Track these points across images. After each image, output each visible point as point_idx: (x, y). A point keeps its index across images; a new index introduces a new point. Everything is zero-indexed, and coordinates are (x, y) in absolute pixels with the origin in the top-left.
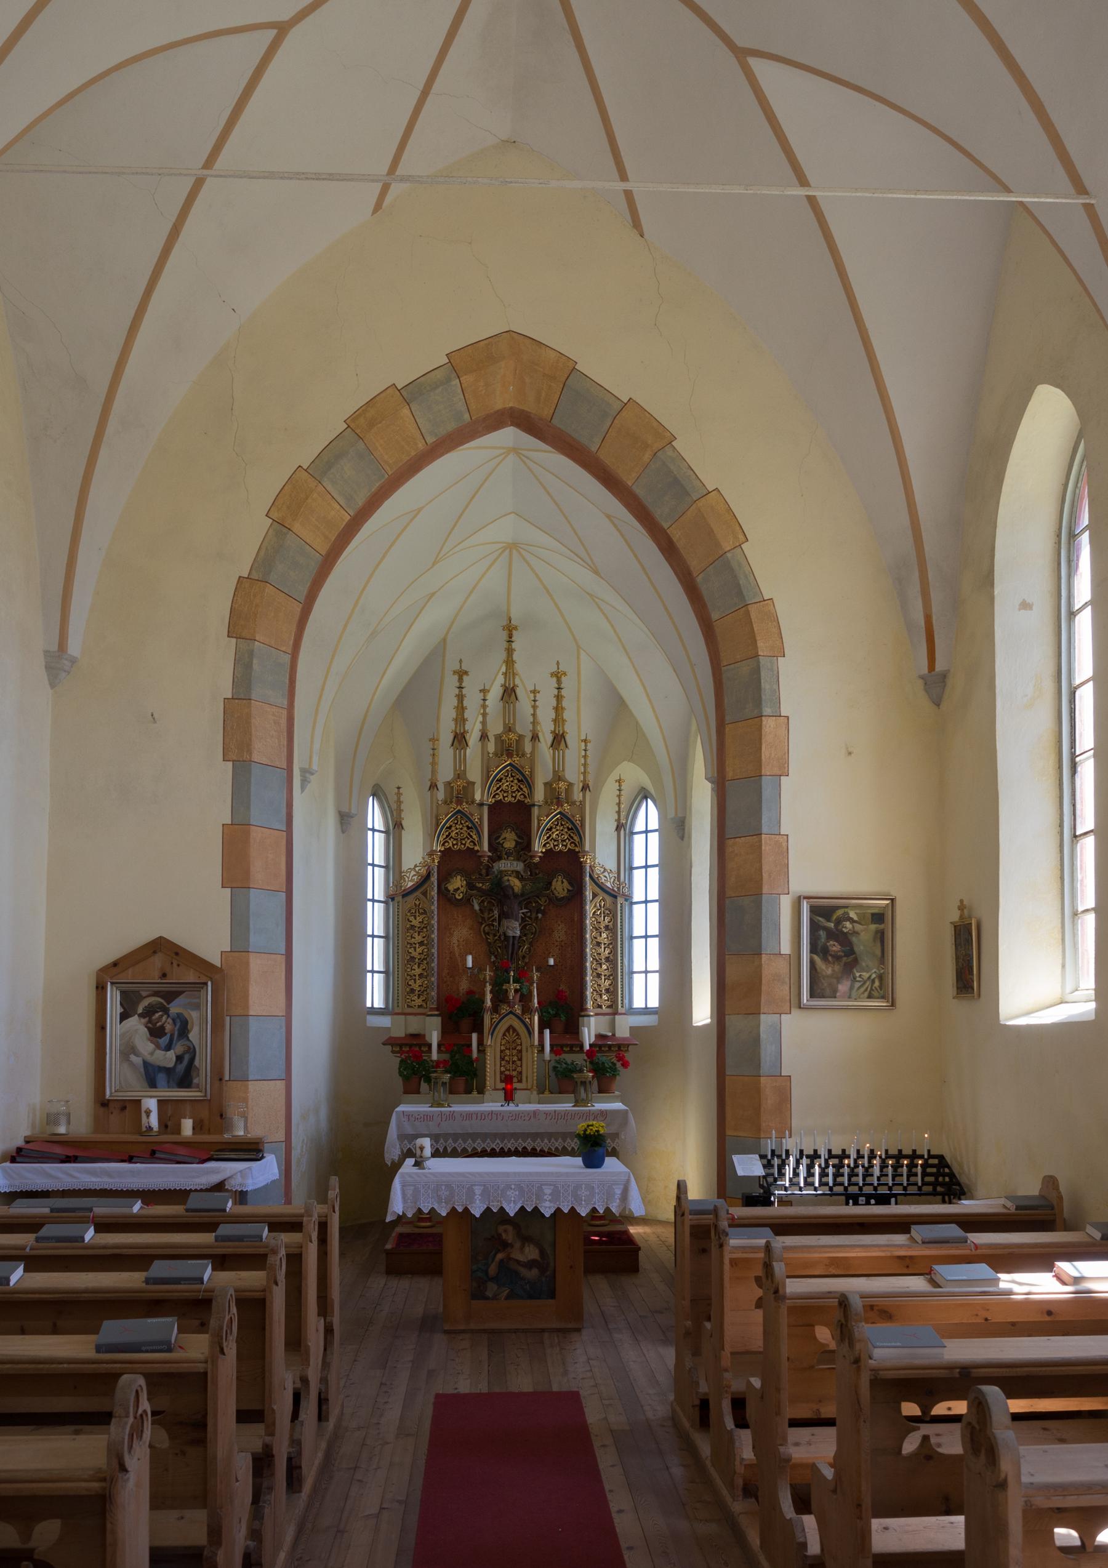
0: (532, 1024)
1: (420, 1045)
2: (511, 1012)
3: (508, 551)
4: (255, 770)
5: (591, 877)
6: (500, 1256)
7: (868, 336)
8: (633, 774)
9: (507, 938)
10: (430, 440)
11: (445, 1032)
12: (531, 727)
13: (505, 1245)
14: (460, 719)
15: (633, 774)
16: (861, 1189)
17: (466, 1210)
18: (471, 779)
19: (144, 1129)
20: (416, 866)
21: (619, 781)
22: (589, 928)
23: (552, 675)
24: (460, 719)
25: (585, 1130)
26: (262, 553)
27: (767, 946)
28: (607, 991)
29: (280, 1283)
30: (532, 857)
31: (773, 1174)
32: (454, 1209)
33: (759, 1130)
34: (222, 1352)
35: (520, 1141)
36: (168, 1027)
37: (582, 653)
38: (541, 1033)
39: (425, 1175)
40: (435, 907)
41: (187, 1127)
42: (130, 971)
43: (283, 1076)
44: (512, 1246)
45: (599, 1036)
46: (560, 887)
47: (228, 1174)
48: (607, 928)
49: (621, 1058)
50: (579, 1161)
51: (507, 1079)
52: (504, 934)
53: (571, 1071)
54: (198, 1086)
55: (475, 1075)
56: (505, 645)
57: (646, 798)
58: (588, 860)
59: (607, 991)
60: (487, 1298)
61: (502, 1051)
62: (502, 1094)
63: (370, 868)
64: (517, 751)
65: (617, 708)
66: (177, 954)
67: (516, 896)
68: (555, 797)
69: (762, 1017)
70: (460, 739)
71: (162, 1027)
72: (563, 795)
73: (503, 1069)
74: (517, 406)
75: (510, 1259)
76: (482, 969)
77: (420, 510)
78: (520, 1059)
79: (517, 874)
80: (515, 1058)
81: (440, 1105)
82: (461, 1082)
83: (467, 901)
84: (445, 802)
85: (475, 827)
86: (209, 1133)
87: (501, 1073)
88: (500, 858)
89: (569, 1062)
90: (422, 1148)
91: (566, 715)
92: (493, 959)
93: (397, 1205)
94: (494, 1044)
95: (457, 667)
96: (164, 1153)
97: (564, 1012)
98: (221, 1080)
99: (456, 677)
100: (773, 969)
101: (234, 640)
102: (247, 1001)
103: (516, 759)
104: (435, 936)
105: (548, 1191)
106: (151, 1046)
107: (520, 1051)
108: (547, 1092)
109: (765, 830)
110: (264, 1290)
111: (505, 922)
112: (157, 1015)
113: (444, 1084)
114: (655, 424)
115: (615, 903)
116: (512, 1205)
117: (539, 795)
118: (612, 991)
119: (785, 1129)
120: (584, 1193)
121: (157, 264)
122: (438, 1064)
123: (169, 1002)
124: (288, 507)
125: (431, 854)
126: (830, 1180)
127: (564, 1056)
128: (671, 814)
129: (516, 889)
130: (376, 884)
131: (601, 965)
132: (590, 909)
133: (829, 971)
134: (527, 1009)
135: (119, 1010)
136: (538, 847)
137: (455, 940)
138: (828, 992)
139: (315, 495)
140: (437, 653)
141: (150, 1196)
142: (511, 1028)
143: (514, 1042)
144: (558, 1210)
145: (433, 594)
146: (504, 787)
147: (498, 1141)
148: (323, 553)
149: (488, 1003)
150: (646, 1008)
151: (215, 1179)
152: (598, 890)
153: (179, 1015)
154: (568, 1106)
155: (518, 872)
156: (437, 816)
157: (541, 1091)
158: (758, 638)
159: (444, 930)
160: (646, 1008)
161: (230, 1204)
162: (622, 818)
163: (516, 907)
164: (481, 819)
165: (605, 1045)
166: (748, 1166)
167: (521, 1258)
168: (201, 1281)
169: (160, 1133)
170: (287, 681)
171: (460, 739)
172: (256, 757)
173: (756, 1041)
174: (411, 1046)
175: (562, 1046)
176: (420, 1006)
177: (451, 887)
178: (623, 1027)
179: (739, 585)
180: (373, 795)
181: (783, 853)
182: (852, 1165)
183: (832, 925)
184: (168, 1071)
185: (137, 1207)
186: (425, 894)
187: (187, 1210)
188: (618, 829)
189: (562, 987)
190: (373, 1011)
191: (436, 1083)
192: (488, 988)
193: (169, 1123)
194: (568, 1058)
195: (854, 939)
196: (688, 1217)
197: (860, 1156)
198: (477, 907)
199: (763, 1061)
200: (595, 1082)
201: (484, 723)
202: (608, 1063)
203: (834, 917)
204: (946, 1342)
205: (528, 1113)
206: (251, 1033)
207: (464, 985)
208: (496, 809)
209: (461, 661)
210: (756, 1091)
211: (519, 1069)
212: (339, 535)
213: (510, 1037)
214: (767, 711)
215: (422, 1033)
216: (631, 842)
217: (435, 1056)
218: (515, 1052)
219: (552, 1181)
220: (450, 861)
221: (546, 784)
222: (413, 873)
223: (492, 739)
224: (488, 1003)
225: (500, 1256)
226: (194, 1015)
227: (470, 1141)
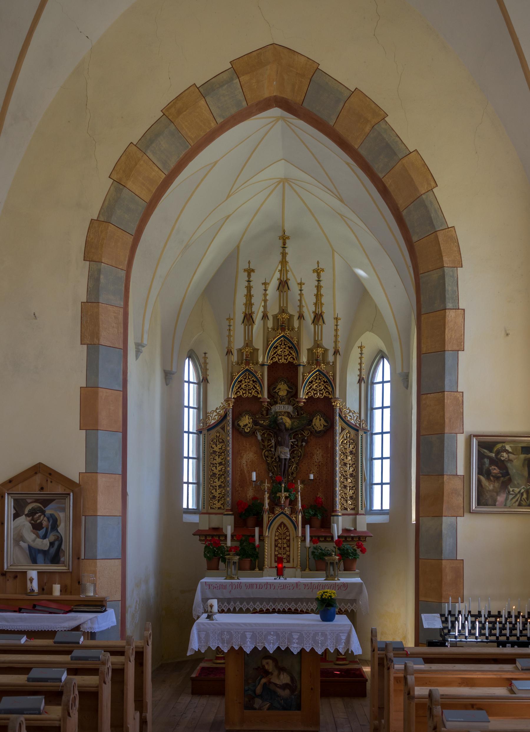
0: (297, 521)
1: (219, 536)
2: (282, 513)
3: (282, 183)
4: (102, 350)
5: (340, 416)
6: (264, 681)
7: (519, 44)
8: (371, 341)
9: (280, 460)
10: (220, 120)
11: (237, 526)
12: (298, 309)
13: (267, 673)
14: (249, 304)
15: (371, 341)
16: (508, 638)
17: (241, 648)
18: (256, 347)
19: (29, 591)
20: (217, 409)
21: (361, 347)
22: (338, 452)
23: (314, 271)
24: (249, 304)
25: (322, 595)
26: (107, 203)
27: (448, 469)
28: (351, 498)
29: (107, 683)
30: (298, 402)
31: (447, 627)
32: (232, 648)
33: (441, 597)
34: (69, 715)
35: (286, 604)
36: (45, 523)
37: (336, 256)
38: (303, 527)
39: (213, 624)
40: (230, 438)
41: (57, 589)
42: (20, 486)
43: (120, 557)
44: (272, 674)
45: (345, 530)
46: (319, 423)
47: (82, 621)
48: (351, 452)
49: (359, 546)
50: (318, 617)
51: (279, 560)
52: (279, 457)
53: (324, 555)
54: (63, 563)
55: (257, 557)
56: (281, 250)
57: (383, 357)
58: (338, 405)
59: (351, 498)
60: (255, 709)
61: (276, 540)
62: (275, 570)
63: (186, 410)
64: (288, 327)
65: (361, 293)
66: (50, 474)
67: (287, 430)
68: (315, 359)
69: (444, 519)
70: (248, 318)
71: (41, 523)
72: (321, 358)
73: (276, 553)
74: (278, 94)
75: (270, 683)
76: (263, 482)
77: (216, 163)
78: (289, 546)
79: (288, 415)
80: (285, 546)
81: (232, 578)
82: (247, 563)
83: (253, 433)
84: (238, 364)
85: (257, 381)
86: (71, 593)
87: (275, 555)
88: (276, 403)
89: (323, 548)
90: (211, 606)
91: (323, 300)
92: (271, 474)
93: (195, 644)
94: (270, 535)
95: (247, 267)
96: (42, 606)
97: (320, 513)
98: (79, 558)
99: (246, 274)
100: (452, 485)
101: (88, 263)
102: (96, 506)
103: (288, 332)
104: (230, 458)
105: (296, 636)
106: (33, 536)
107: (289, 540)
108: (307, 570)
109: (447, 388)
110: (97, 687)
111: (279, 449)
112: (37, 515)
113: (234, 563)
114: (373, 106)
115: (357, 435)
116: (271, 645)
117: (304, 359)
118: (354, 498)
119: (459, 596)
120: (320, 638)
121: (35, 16)
122: (231, 548)
123: (45, 508)
124: (124, 171)
125: (227, 400)
126: (487, 632)
127: (320, 544)
128: (399, 370)
129: (287, 425)
130: (190, 420)
131: (347, 479)
132: (339, 439)
133: (491, 487)
134: (294, 511)
135: (13, 511)
136: (302, 395)
137: (244, 461)
138: (490, 502)
139: (142, 162)
140: (233, 256)
141: (32, 634)
142: (282, 524)
143: (284, 533)
144: (303, 650)
145: (228, 217)
146: (279, 352)
147: (271, 603)
148: (148, 201)
149: (267, 506)
150: (382, 509)
151: (74, 624)
152: (345, 426)
153: (52, 515)
154: (321, 580)
155: (289, 413)
156: (232, 373)
157: (303, 569)
158: (444, 254)
159: (236, 454)
160: (382, 509)
161: (82, 639)
162: (362, 374)
163: (287, 437)
164: (262, 375)
165: (349, 537)
166: (432, 622)
167: (278, 682)
168: (60, 680)
169: (39, 594)
170: (123, 289)
171: (248, 318)
172: (102, 342)
173: (439, 535)
174: (213, 536)
175: (319, 537)
176: (219, 508)
177: (242, 424)
178: (363, 523)
179: (431, 218)
180: (189, 357)
181: (460, 404)
182: (503, 622)
183: (493, 455)
184: (45, 553)
185: (24, 640)
186: (223, 428)
187: (55, 643)
188: (360, 382)
189: (320, 495)
190: (188, 511)
191: (229, 562)
192: (267, 495)
193: (45, 587)
194: (323, 545)
195: (509, 465)
196: (377, 652)
197: (510, 615)
198: (259, 438)
199: (444, 549)
200: (342, 563)
201: (265, 307)
202: (350, 550)
203: (495, 449)
204: (490, 718)
205: (292, 584)
206: (99, 529)
207: (250, 493)
208: (273, 367)
209: (249, 262)
210: (439, 570)
211: (288, 553)
212: (158, 188)
213: (282, 530)
214: (449, 305)
215: (221, 527)
216: (372, 389)
217: (229, 543)
218: (285, 541)
219: (301, 631)
220: (240, 405)
221: (308, 350)
222: (215, 414)
223: (271, 318)
224: (267, 506)
225: (264, 681)
226: (62, 515)
227: (251, 603)
